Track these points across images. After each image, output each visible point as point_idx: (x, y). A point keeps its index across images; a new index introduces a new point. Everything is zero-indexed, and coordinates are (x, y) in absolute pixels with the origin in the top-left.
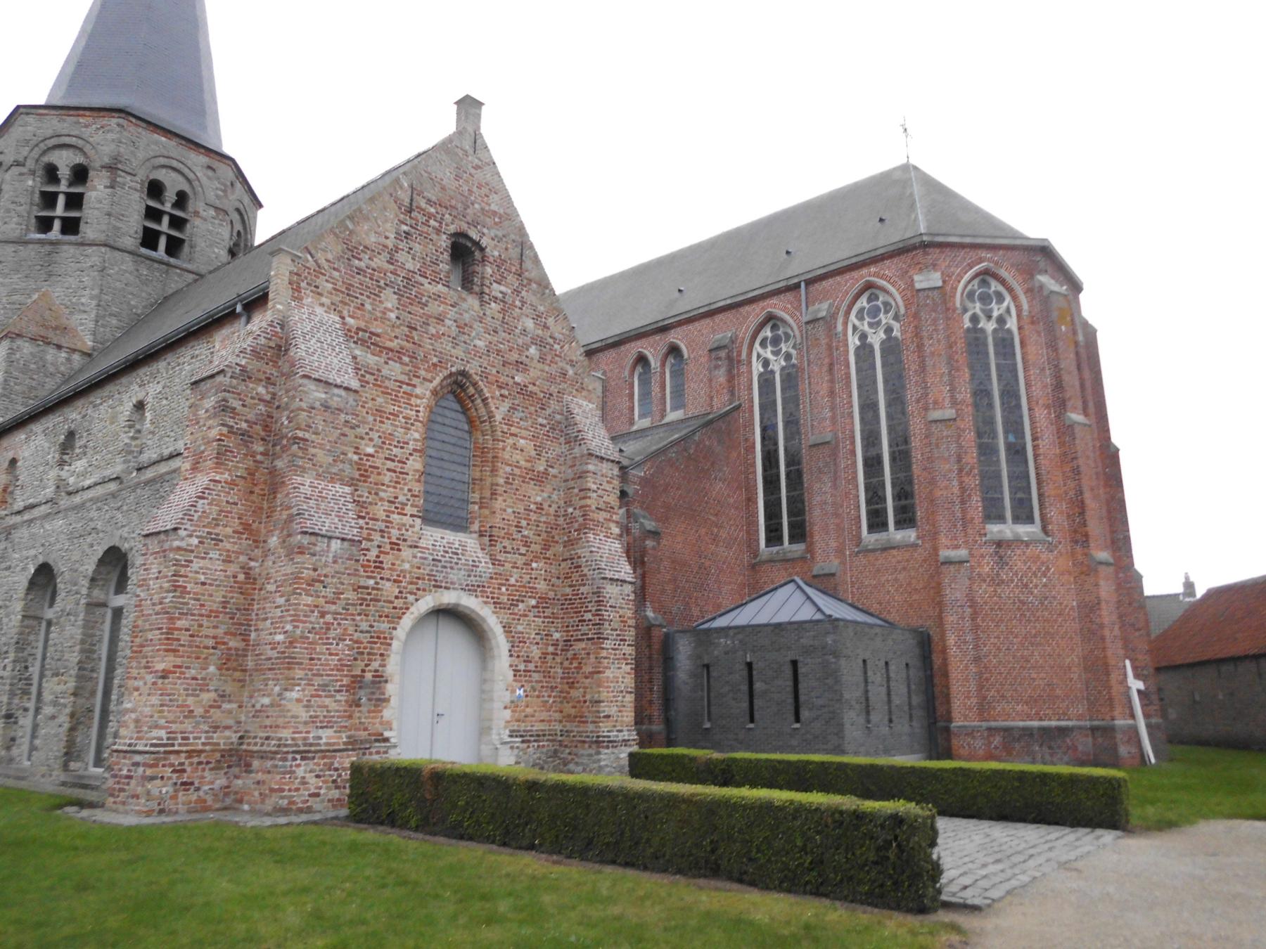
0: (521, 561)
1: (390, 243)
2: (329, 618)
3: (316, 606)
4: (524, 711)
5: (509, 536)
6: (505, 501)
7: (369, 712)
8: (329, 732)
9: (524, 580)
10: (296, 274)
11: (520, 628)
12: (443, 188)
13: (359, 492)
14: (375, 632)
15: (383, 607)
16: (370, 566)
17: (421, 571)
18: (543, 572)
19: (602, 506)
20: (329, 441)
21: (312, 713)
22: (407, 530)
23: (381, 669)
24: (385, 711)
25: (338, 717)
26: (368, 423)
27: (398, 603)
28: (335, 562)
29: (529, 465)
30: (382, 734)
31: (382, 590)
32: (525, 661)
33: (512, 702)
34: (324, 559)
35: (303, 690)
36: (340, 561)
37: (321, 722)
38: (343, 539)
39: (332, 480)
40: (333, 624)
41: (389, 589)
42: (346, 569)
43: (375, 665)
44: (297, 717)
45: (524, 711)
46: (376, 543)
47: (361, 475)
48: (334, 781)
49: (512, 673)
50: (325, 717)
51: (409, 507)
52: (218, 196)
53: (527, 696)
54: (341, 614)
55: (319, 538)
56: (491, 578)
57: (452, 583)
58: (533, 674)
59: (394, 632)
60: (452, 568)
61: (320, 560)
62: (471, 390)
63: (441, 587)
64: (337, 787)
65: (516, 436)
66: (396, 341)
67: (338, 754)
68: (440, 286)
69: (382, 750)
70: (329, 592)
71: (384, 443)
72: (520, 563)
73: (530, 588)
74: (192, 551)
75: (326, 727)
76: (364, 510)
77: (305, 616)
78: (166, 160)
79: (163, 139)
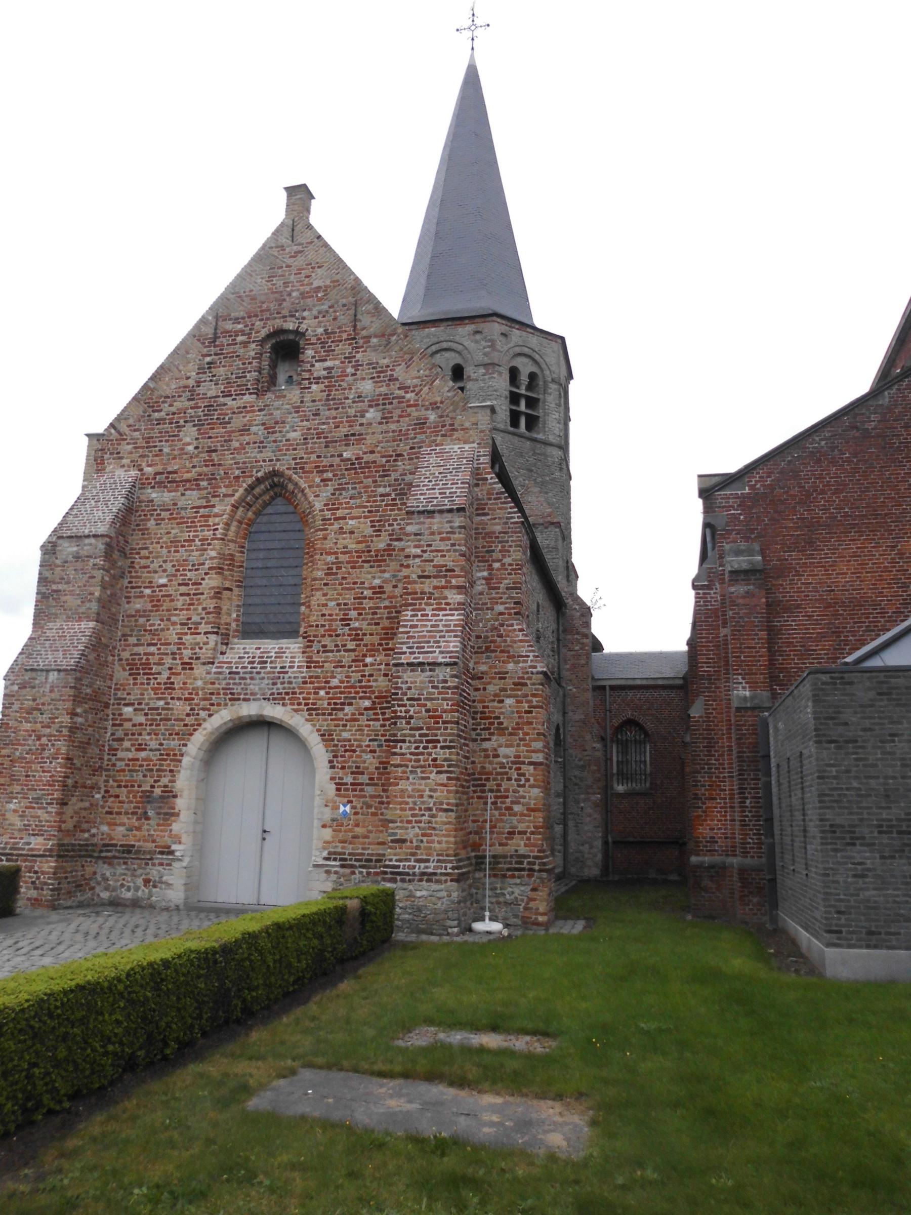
0: (347, 658)
1: (191, 382)
2: (44, 740)
3: (34, 731)
4: (351, 831)
5: (332, 633)
6: (325, 595)
7: (158, 825)
8: (40, 839)
9: (352, 680)
10: (101, 450)
11: (345, 735)
12: (253, 299)
13: (151, 622)
14: (164, 749)
15: (174, 725)
16: (161, 689)
17: (217, 686)
18: (383, 667)
19: (429, 569)
20: (79, 587)
21: (26, 822)
22: (201, 648)
23: (170, 784)
24: (174, 824)
25: (48, 827)
26: (162, 557)
27: (189, 720)
28: (51, 691)
29: (361, 546)
30: (169, 847)
31: (172, 709)
32: (352, 773)
33: (333, 820)
34: (41, 690)
35: (20, 803)
36: (56, 689)
37: (33, 830)
38: (59, 671)
39: (80, 619)
40: (47, 745)
41: (180, 708)
42: (61, 696)
43: (165, 781)
44: (13, 825)
45: (351, 831)
46: (167, 666)
47: (153, 606)
48: (33, 883)
49: (334, 786)
50: (36, 826)
51: (203, 625)
52: (485, 354)
53: (356, 813)
54: (55, 736)
55: (39, 673)
56: (305, 683)
57: (252, 694)
58: (366, 788)
59: (184, 749)
60: (252, 678)
61: (39, 692)
62: (291, 487)
63: (239, 699)
64: (36, 888)
65: (344, 518)
66: (194, 470)
67: (38, 859)
68: (245, 397)
69: (165, 862)
70: (45, 718)
71: (178, 570)
72: (345, 662)
73: (361, 687)
74: (13, 696)
75: (37, 835)
76: (156, 637)
77: (24, 740)
78: (437, 345)
79: (433, 329)
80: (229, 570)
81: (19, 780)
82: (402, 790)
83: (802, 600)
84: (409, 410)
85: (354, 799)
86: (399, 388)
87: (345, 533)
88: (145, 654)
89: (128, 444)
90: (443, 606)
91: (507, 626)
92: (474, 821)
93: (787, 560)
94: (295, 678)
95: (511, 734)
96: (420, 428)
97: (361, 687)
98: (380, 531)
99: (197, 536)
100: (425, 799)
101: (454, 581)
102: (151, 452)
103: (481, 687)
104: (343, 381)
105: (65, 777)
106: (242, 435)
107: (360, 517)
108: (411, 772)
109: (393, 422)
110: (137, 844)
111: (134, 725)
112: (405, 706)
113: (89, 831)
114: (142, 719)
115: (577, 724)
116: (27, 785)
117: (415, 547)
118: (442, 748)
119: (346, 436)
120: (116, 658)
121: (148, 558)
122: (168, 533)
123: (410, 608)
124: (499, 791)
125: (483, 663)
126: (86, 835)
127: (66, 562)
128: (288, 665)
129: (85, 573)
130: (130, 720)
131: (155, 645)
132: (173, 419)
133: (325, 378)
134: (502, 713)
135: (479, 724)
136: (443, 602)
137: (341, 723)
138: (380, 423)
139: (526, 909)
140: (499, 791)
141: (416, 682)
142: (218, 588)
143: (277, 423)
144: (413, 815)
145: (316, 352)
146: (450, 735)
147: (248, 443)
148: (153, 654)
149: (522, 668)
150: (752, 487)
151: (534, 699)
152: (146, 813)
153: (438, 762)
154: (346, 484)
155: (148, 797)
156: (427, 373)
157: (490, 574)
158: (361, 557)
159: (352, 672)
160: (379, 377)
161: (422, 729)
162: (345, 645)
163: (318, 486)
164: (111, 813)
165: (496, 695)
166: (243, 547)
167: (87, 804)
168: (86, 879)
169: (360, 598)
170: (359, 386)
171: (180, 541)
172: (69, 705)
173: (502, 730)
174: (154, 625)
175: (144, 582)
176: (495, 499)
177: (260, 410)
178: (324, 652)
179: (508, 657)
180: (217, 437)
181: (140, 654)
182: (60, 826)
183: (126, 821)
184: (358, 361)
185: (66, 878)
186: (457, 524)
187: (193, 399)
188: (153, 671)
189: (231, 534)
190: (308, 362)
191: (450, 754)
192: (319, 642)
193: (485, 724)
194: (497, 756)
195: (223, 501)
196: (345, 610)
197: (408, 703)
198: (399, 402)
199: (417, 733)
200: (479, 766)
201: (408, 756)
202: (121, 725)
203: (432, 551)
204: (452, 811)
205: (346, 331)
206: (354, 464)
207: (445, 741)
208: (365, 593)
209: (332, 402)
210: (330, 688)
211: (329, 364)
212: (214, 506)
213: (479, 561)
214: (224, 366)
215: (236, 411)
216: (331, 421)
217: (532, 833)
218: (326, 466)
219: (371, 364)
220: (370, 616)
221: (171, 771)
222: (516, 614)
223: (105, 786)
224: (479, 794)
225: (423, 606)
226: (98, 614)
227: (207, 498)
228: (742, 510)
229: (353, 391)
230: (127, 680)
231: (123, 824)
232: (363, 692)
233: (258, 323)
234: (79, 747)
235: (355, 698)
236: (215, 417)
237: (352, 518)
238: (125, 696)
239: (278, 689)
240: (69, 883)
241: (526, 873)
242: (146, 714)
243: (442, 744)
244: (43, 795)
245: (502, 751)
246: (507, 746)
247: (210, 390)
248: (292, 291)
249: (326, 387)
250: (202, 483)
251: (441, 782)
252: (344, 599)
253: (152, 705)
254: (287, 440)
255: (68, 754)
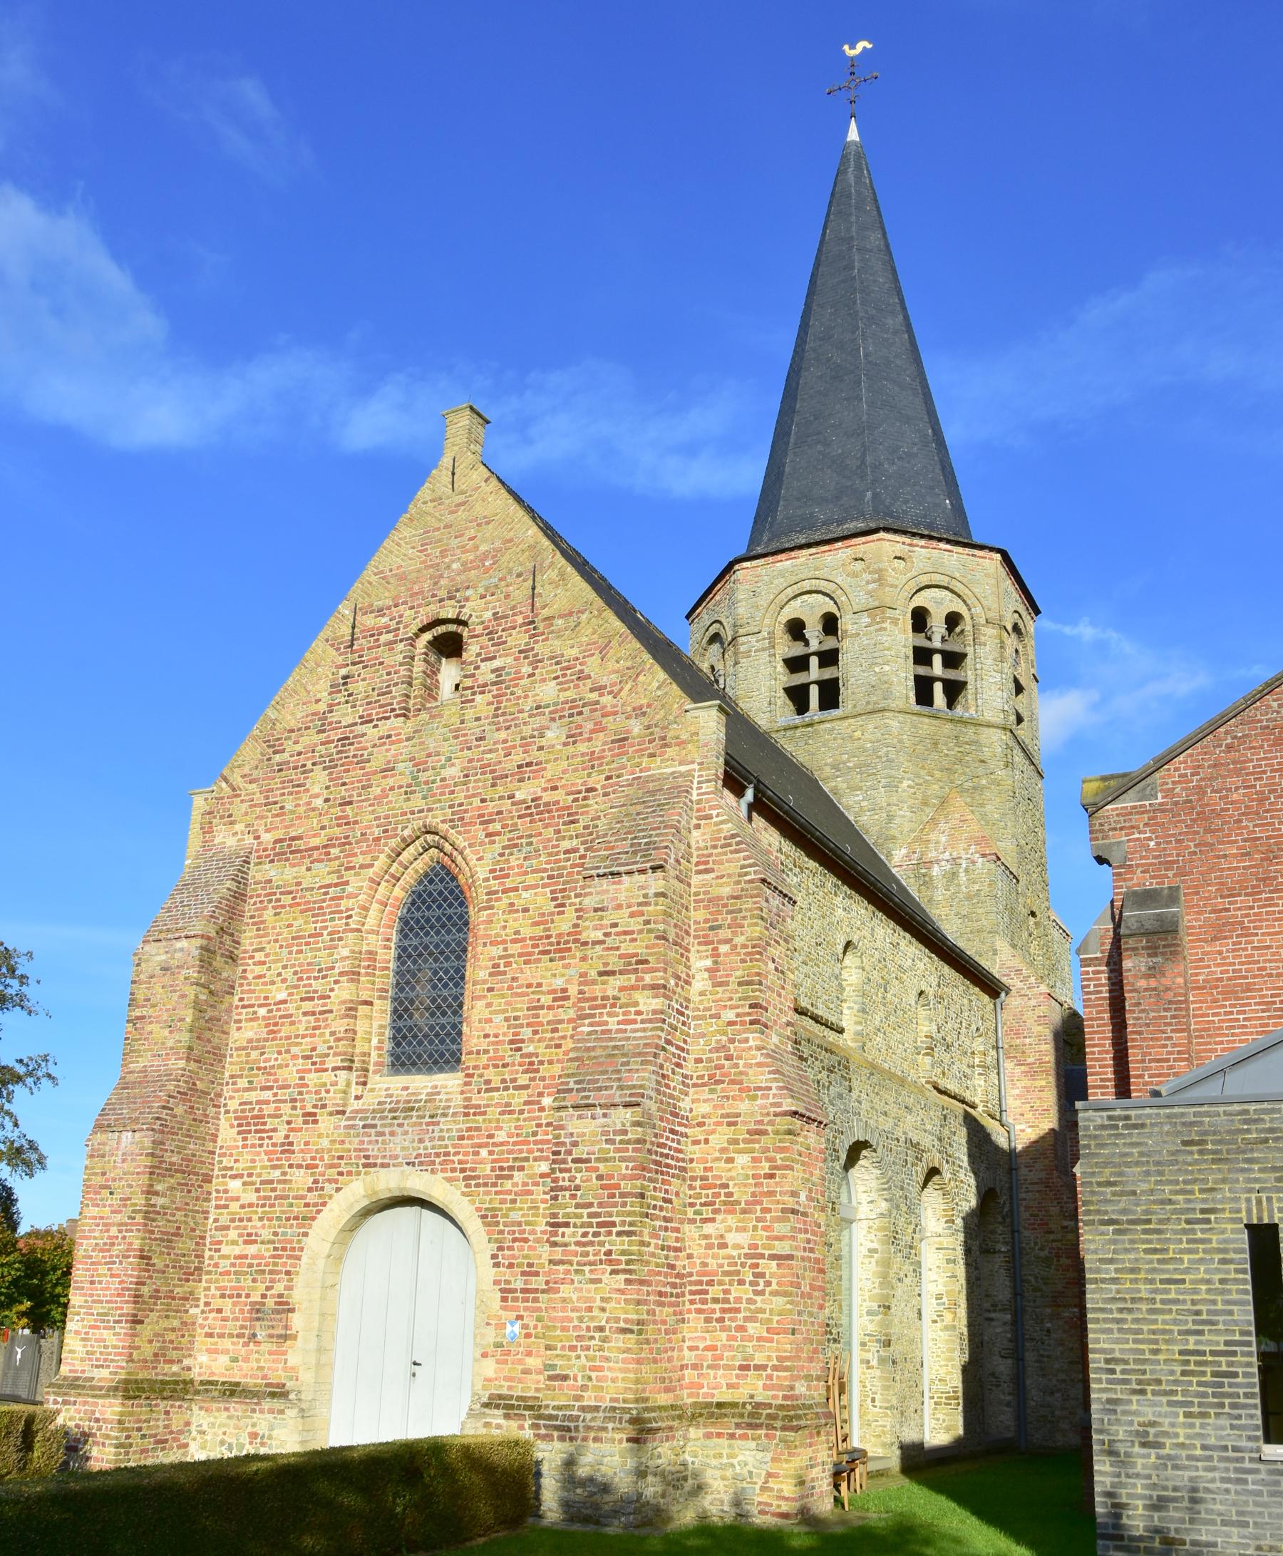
1: (322, 707)
2: (114, 1231)
4: (520, 1362)
10: (209, 813)
14: (279, 1241)
19: (614, 963)
20: (167, 1010)
22: (328, 1092)
25: (116, 1354)
27: (312, 1198)
28: (123, 1161)
29: (538, 931)
32: (523, 1274)
43: (279, 1288)
46: (285, 1118)
49: (499, 1295)
50: (101, 1353)
53: (528, 1336)
54: (126, 1224)
63: (375, 1165)
65: (516, 889)
71: (300, 979)
73: (536, 1143)
75: (102, 1366)
80: (367, 974)
81: (83, 1288)
82: (564, 1300)
83: (1254, 977)
84: (605, 720)
85: (525, 1314)
86: (592, 690)
87: (517, 911)
88: (258, 1102)
89: (242, 801)
90: (633, 1017)
91: (740, 1042)
92: (691, 1349)
93: (1228, 910)
94: (448, 1130)
95: (744, 1212)
96: (620, 747)
97: (536, 1143)
98: (563, 905)
99: (326, 928)
100: (596, 1313)
101: (648, 979)
102: (270, 811)
103: (702, 1138)
104: (516, 686)
105: (137, 1283)
106: (384, 777)
107: (536, 886)
108: (577, 1271)
109: (583, 741)
110: (243, 1380)
111: (242, 1207)
112: (569, 1170)
113: (180, 1361)
114: (251, 1197)
115: (1036, 1188)
116: (92, 1295)
117: (595, 928)
118: (619, 1234)
119: (520, 767)
120: (222, 1110)
121: (264, 963)
122: (290, 926)
123: (587, 1021)
124: (727, 1301)
125: (705, 1101)
126: (175, 1368)
127: (152, 977)
128: (440, 1112)
129: (175, 991)
130: (237, 1199)
131: (270, 1088)
132: (298, 761)
133: (494, 684)
134: (731, 1178)
135: (699, 1196)
136: (633, 1010)
137: (509, 1197)
138: (565, 744)
139: (763, 1489)
140: (727, 1301)
141: (584, 1134)
142: (352, 1001)
143: (429, 755)
144: (579, 1338)
145: (481, 648)
146: (629, 1214)
147: (392, 789)
148: (267, 1102)
149: (762, 1107)
150: (1168, 793)
151: (778, 1156)
152: (254, 1335)
153: (614, 1257)
154: (519, 838)
155: (258, 1311)
156: (629, 664)
157: (716, 962)
158: (536, 946)
159: (525, 1120)
160: (564, 675)
161: (590, 1205)
162: (514, 1080)
163: (482, 844)
164: (210, 1335)
165: (723, 1150)
166: (388, 940)
167: (176, 1323)
168: (171, 1432)
169: (535, 1007)
170: (538, 691)
171: (303, 937)
172: (145, 1179)
173: (731, 1205)
174: (269, 1060)
175: (258, 998)
176: (723, 846)
177: (408, 739)
178: (487, 1091)
179: (740, 1090)
180: (353, 783)
181: (251, 1103)
182: (131, 1355)
183: (231, 1347)
184: (537, 655)
185: (139, 1429)
186: (651, 892)
187: (324, 731)
188: (267, 1127)
189: (371, 922)
190: (471, 663)
191: (630, 1243)
192: (481, 1076)
193: (707, 1196)
194: (723, 1246)
195: (359, 874)
196: (516, 1026)
197: (574, 1166)
198: (592, 711)
199: (585, 1211)
200: (698, 1262)
201: (573, 1247)
202: (226, 1207)
203: (618, 934)
204: (631, 1331)
205: (521, 613)
206: (528, 808)
207: (623, 1223)
208: (543, 1000)
209: (501, 719)
210: (495, 1144)
211: (497, 663)
212: (347, 883)
213: (700, 944)
214: (364, 680)
215: (378, 742)
216: (500, 746)
217: (775, 1368)
218: (491, 814)
219: (553, 658)
220: (549, 1035)
221: (288, 1273)
222: (752, 1023)
223: (206, 1296)
224: (699, 1306)
225: (605, 1018)
226: (190, 1048)
227: (339, 871)
228: (1153, 832)
229: (529, 700)
230: (235, 1140)
231: (226, 1352)
232: (539, 1150)
233: (408, 613)
234: (162, 1240)
235: (527, 1159)
236: (351, 754)
237: (527, 888)
238: (232, 1164)
239: (426, 1148)
240: (144, 1436)
241: (762, 1432)
242: (257, 1190)
243: (619, 1229)
244: (110, 1309)
245: (731, 1238)
246: (738, 1230)
247: (345, 715)
248: (453, 561)
249: (494, 697)
250: (332, 851)
251: (617, 1286)
252: (515, 1010)
253: (265, 1177)
254: (442, 780)
255: (142, 1250)
